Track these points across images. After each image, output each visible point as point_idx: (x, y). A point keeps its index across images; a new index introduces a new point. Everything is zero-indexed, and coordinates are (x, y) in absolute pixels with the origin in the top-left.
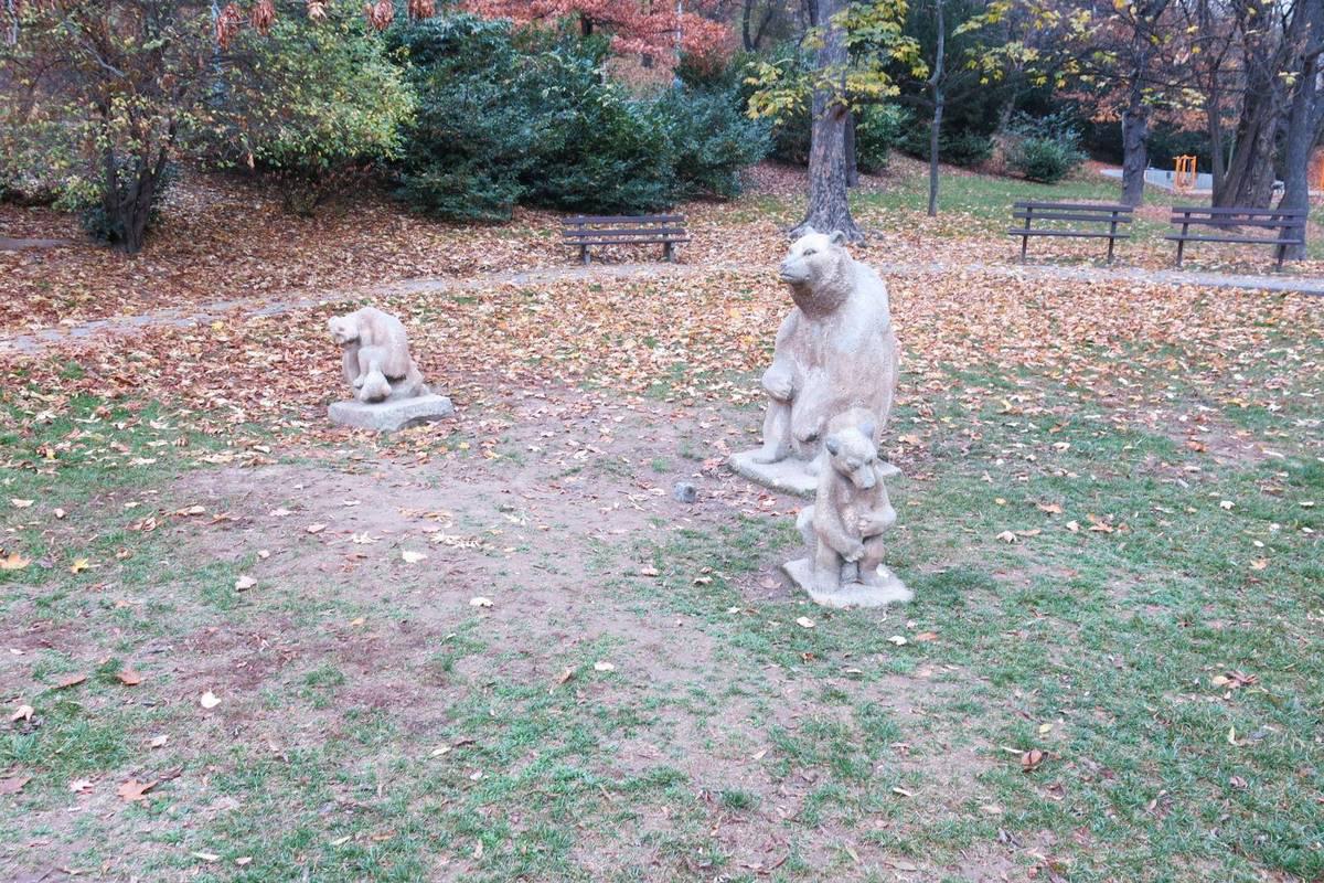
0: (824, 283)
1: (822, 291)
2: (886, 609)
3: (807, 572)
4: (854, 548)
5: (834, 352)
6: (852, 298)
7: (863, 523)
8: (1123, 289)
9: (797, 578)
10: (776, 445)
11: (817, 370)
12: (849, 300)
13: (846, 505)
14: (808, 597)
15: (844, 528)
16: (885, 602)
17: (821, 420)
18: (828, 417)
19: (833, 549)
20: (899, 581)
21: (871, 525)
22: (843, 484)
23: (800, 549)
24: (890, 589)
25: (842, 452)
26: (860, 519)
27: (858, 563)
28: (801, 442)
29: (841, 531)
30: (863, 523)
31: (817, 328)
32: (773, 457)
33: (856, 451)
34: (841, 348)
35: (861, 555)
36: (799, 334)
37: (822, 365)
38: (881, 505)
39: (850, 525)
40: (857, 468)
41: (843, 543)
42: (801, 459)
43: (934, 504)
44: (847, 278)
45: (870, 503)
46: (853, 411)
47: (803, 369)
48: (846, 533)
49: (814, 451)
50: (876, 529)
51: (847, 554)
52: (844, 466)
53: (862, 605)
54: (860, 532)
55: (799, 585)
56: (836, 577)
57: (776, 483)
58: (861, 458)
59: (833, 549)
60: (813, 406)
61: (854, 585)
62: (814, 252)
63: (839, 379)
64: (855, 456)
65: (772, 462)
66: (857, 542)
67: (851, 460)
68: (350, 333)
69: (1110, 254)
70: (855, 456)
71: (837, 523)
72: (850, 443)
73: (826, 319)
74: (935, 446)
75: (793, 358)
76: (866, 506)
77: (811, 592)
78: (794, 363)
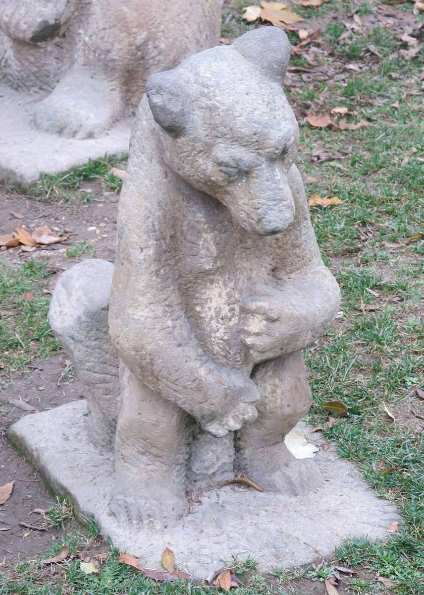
2: (331, 572)
3: (86, 452)
4: (232, 397)
7: (256, 325)
9: (61, 474)
13: (205, 276)
14: (101, 540)
15: (202, 339)
16: (326, 550)
19: (168, 403)
20: (346, 468)
21: (281, 330)
22: (198, 216)
23: (50, 366)
24: (329, 498)
25: (197, 124)
26: (246, 312)
27: (237, 437)
28: (19, 42)
29: (192, 351)
30: (256, 325)
33: (242, 125)
35: (251, 413)
38: (304, 262)
39: (219, 332)
40: (244, 173)
41: (200, 387)
43: (371, 201)
45: (268, 262)
48: (208, 354)
49: (51, 64)
50: (293, 337)
51: (213, 417)
52: (207, 167)
53: (266, 565)
54: (246, 349)
55: (65, 495)
56: (176, 478)
58: (255, 142)
59: (168, 403)
61: (227, 494)
64: (237, 140)
66: (238, 380)
67: (225, 152)
70: (237, 140)
71: (182, 329)
72: (223, 99)
74: (337, 31)
76: (260, 271)
77: (109, 526)
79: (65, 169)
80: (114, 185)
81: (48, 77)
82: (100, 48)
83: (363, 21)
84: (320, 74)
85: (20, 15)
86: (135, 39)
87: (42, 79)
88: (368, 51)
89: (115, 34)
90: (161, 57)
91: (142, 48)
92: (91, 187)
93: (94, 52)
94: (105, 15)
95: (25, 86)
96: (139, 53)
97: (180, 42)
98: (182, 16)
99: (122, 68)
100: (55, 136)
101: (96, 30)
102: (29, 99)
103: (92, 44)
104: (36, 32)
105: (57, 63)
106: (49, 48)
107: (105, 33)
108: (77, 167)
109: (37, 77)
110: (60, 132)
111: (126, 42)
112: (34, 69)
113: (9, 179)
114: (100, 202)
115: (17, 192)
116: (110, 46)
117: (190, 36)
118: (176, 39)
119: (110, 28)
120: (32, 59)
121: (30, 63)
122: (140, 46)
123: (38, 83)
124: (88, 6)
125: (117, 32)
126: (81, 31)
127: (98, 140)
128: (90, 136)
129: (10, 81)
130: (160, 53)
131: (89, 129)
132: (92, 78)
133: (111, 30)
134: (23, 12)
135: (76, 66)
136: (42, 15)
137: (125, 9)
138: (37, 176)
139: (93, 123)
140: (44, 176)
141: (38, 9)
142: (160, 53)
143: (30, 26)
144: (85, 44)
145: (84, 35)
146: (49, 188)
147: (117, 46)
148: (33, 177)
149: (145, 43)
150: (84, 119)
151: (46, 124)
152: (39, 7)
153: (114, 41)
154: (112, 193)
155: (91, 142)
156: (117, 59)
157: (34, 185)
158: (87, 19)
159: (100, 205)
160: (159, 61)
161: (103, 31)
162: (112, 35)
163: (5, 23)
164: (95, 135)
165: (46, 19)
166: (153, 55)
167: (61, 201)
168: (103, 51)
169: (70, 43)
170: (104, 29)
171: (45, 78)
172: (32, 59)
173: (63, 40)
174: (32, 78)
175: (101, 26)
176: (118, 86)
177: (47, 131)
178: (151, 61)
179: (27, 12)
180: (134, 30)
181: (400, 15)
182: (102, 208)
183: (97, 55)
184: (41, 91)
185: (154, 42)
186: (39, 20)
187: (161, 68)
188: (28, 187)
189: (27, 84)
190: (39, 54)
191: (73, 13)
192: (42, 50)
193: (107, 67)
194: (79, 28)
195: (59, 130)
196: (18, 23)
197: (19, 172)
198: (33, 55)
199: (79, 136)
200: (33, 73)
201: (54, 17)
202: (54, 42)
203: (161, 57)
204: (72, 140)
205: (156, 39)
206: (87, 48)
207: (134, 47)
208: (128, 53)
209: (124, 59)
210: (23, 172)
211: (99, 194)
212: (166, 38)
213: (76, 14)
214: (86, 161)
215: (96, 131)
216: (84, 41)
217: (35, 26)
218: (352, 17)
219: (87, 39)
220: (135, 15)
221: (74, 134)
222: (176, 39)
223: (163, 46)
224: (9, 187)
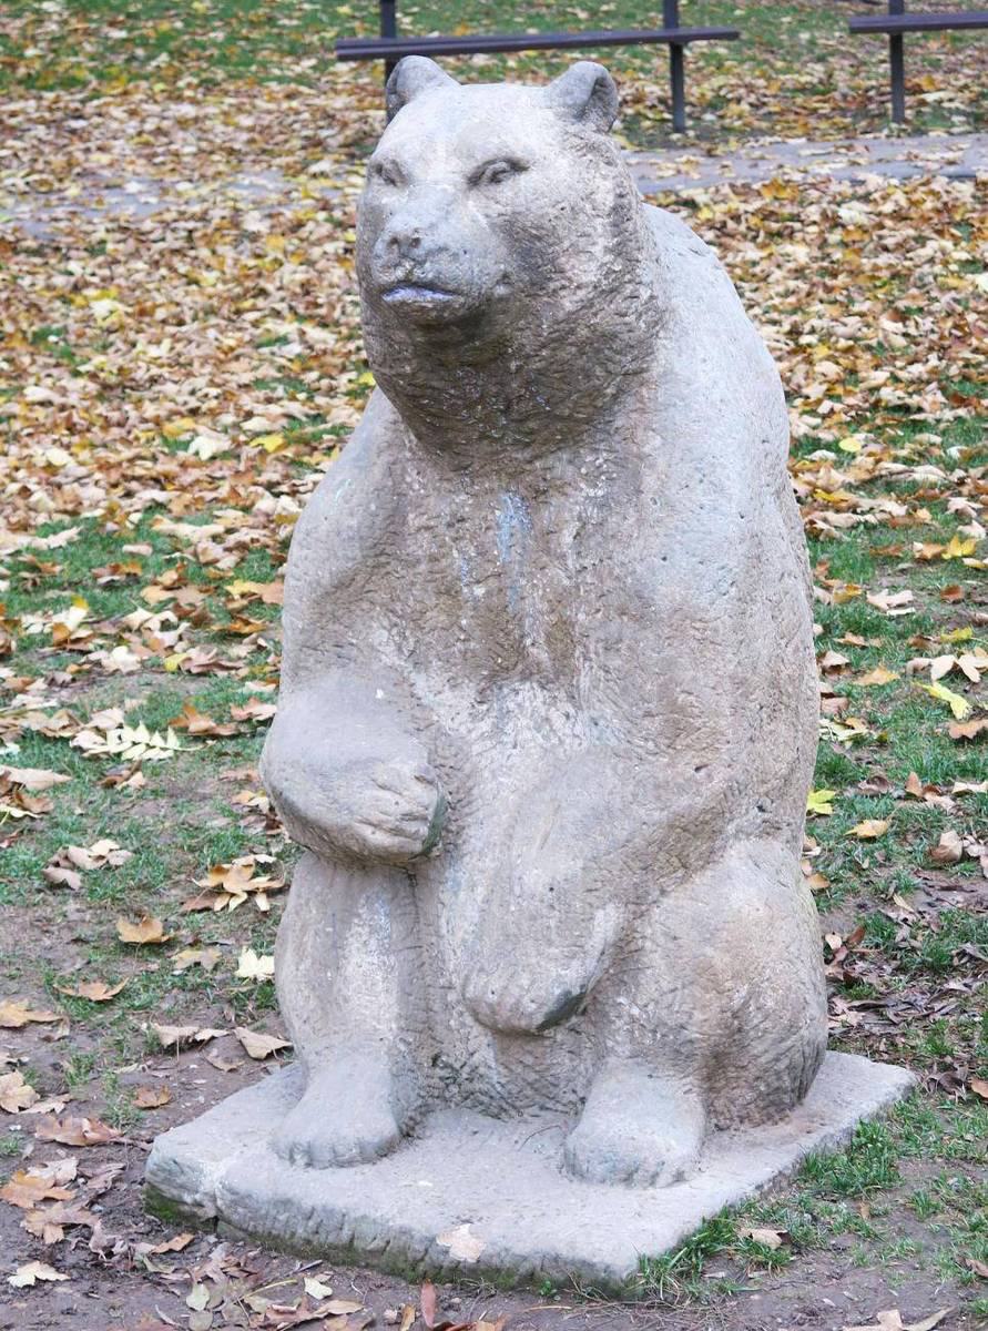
0: (568, 303)
1: (559, 340)
5: (637, 607)
6: (666, 354)
8: (813, 213)
10: (382, 1067)
11: (527, 697)
12: (656, 370)
17: (606, 923)
18: (638, 904)
31: (506, 514)
32: (387, 1126)
34: (667, 591)
36: (420, 545)
37: (558, 676)
42: (498, 1108)
44: (646, 272)
46: (735, 854)
47: (452, 705)
57: (464, 1246)
60: (566, 865)
62: (516, 167)
63: (677, 726)
65: (386, 1150)
68: (235, 1269)
69: (677, 100)
73: (560, 465)
75: (390, 657)
78: (403, 681)
79: (673, 1243)
80: (761, 1258)
81: (556, 1086)
82: (666, 1024)
83: (912, 904)
84: (905, 1006)
85: (521, 987)
86: (731, 999)
87: (544, 1091)
88: (963, 954)
89: (694, 996)
90: (768, 1024)
91: (740, 1014)
92: (721, 1268)
93: (654, 1032)
94: (671, 966)
95: (514, 1107)
96: (736, 1022)
97: (796, 993)
98: (792, 949)
99: (707, 1053)
100: (620, 1188)
101: (656, 995)
102: (523, 1129)
103: (648, 1020)
104: (552, 1012)
105: (571, 1060)
106: (559, 1037)
107: (674, 998)
108: (687, 1237)
109: (536, 1090)
110: (628, 1179)
111: (715, 1007)
112: (532, 1077)
113: (579, 1276)
114: (752, 1292)
115: (601, 1297)
116: (685, 1018)
117: (806, 980)
118: (789, 988)
119: (684, 987)
120: (529, 1060)
121: (526, 1066)
122: (739, 1010)
123: (538, 1098)
124: (636, 955)
125: (698, 992)
126: (621, 1000)
127: (693, 1183)
128: (679, 1178)
129: (482, 1104)
130: (766, 1018)
131: (677, 1165)
132: (650, 1076)
133: (686, 991)
134: (525, 982)
135: (612, 1060)
136: (561, 983)
137: (709, 951)
138: (635, 1264)
139: (679, 1154)
140: (643, 1262)
141: (554, 974)
142: (766, 1018)
143: (541, 1005)
144: (633, 1020)
145: (628, 1006)
146: (658, 1281)
147: (698, 1016)
148: (629, 1266)
149: (746, 1004)
150: (663, 1151)
151: (600, 1170)
152: (554, 970)
153: (694, 1009)
154: (763, 1272)
155: (683, 1188)
156: (697, 1039)
157: (632, 1280)
158: (635, 977)
159: (756, 1297)
160: (765, 1031)
161: (670, 996)
162: (688, 1000)
163: (490, 1005)
164: (686, 1175)
165: (568, 987)
166: (756, 1021)
167: (688, 1302)
168: (671, 1029)
169: (594, 1024)
170: (673, 991)
171: (551, 1088)
172: (529, 1060)
173: (582, 1019)
174: (529, 1092)
175: (665, 986)
176: (696, 1082)
177: (603, 1181)
178: (752, 1033)
179: (533, 982)
180: (728, 985)
181: (964, 883)
182: (761, 1302)
183: (659, 1036)
184: (543, 1113)
185: (757, 1001)
186: (558, 992)
187: (770, 1042)
188: (622, 1285)
189: (518, 1104)
190: (541, 1050)
191: (607, 971)
192: (547, 1043)
193: (679, 1055)
194: (619, 995)
195: (624, 1176)
196: (518, 1002)
197: (601, 1263)
198: (530, 1053)
199: (662, 1180)
200: (529, 1084)
201: (580, 982)
202: (567, 1025)
203: (768, 1024)
204: (651, 1191)
205: (760, 993)
206: (636, 1026)
207: (729, 1014)
208: (719, 1025)
209: (710, 1036)
210: (608, 1260)
211: (741, 1276)
212: (774, 990)
213: (611, 971)
214: (698, 1224)
215: (685, 1168)
216: (631, 1016)
217: (550, 1004)
218: (892, 899)
219: (635, 1011)
220: (727, 959)
221: (653, 1179)
222: (789, 988)
223: (770, 1004)
224: (584, 1292)
